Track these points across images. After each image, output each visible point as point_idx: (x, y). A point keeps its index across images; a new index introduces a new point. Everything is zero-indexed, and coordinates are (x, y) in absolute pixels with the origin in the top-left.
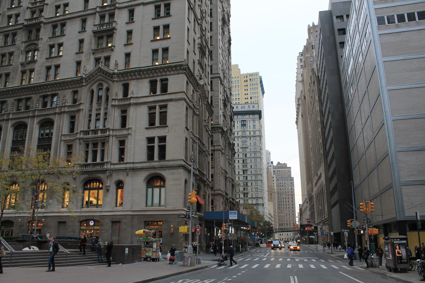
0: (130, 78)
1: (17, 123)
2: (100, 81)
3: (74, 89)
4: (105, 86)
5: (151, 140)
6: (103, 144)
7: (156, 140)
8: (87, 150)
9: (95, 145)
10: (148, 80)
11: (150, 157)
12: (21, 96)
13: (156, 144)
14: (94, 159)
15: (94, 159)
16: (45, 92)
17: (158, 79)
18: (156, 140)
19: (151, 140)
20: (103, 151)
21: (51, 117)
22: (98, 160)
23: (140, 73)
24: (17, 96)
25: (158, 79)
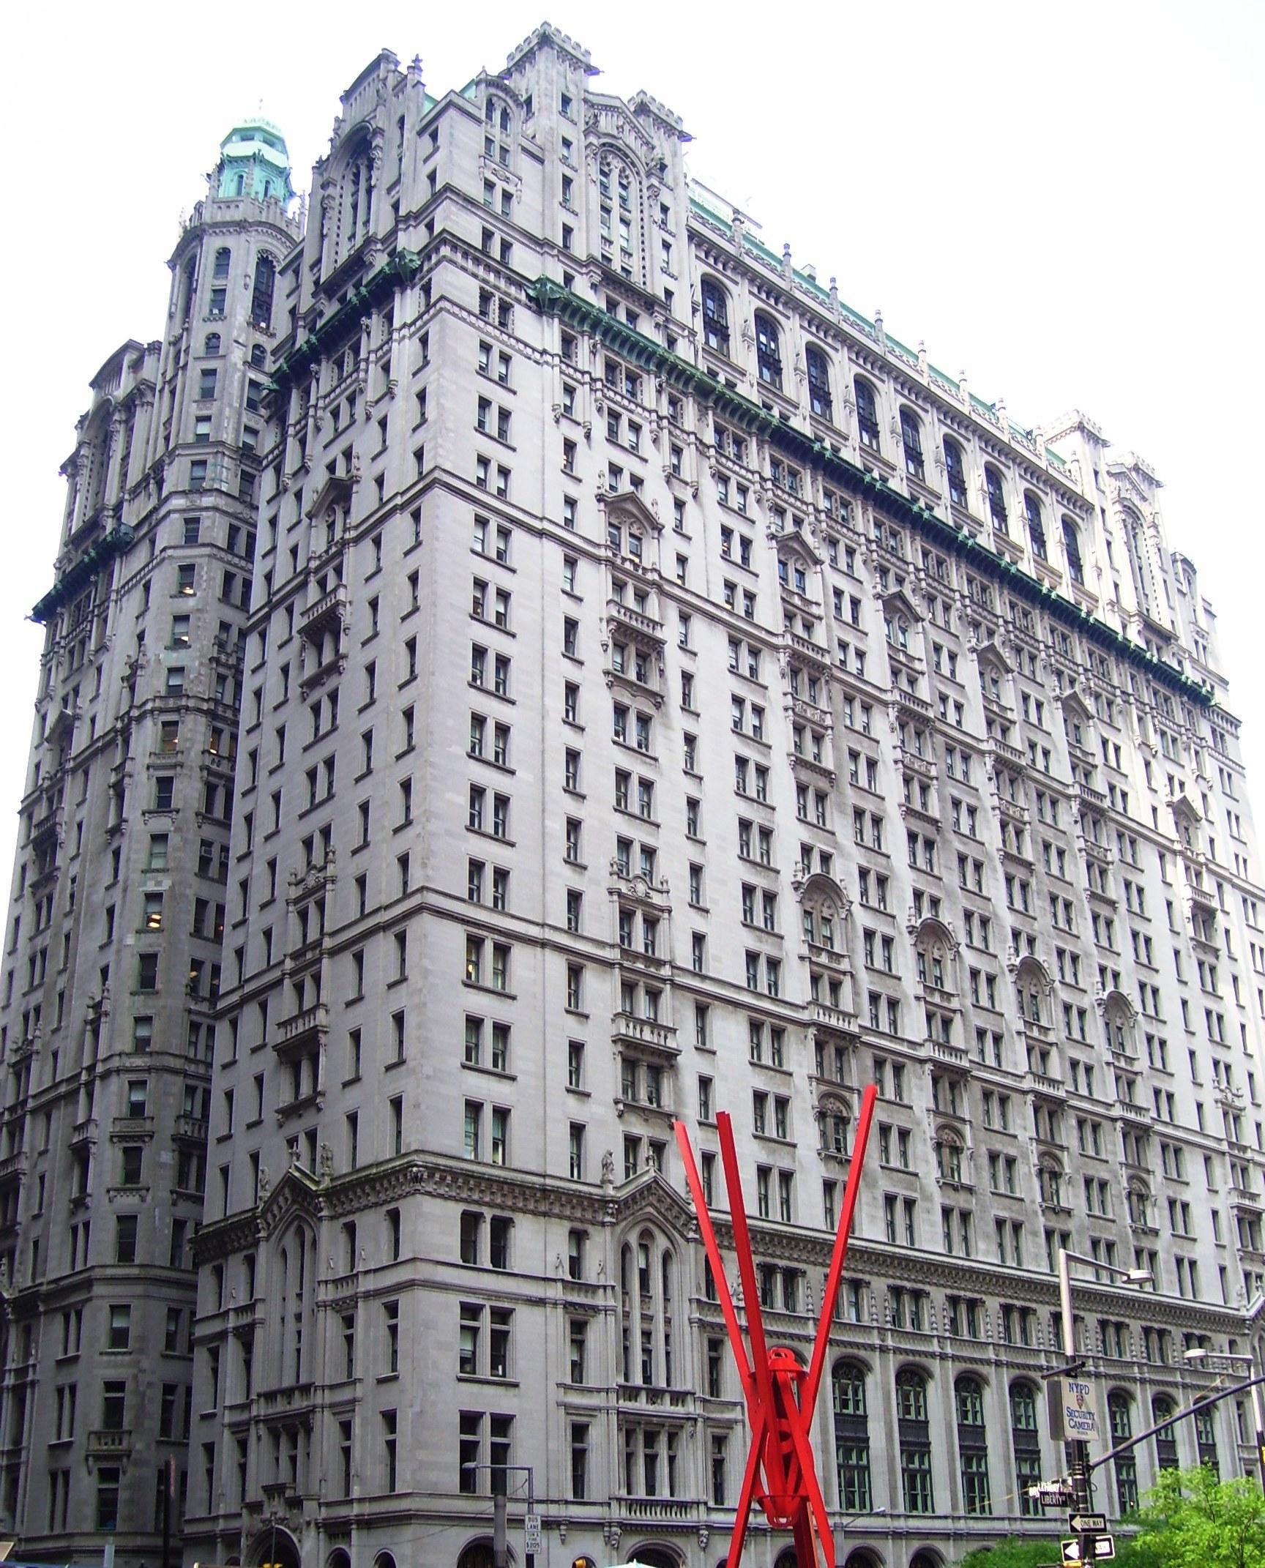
0: (556, 1210)
1: (966, 1371)
2: (651, 1226)
3: (578, 1225)
4: (661, 1243)
5: (469, 1421)
6: (672, 1438)
7: (486, 1424)
8: (347, 1444)
9: (650, 1439)
10: (461, 1207)
11: (468, 1481)
12: (780, 1257)
13: (485, 1437)
14: (651, 1489)
15: (651, 1489)
16: (772, 1256)
17: (488, 1213)
18: (486, 1424)
19: (469, 1421)
20: (672, 1459)
21: (984, 1370)
22: (664, 1493)
23: (543, 1198)
24: (854, 1270)
25: (488, 1213)
